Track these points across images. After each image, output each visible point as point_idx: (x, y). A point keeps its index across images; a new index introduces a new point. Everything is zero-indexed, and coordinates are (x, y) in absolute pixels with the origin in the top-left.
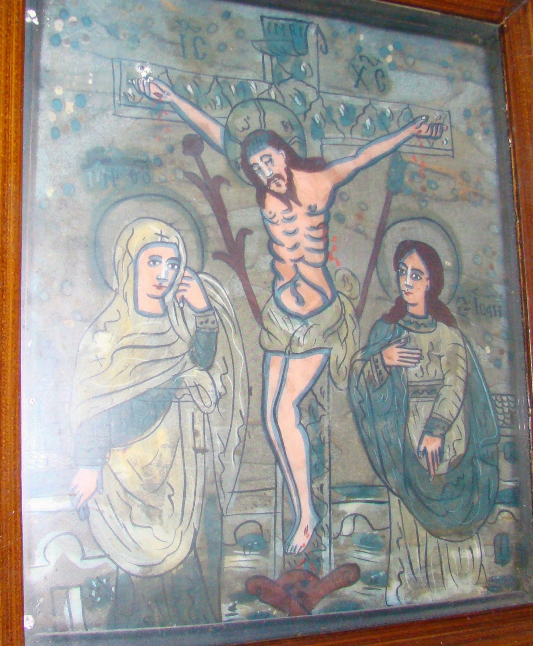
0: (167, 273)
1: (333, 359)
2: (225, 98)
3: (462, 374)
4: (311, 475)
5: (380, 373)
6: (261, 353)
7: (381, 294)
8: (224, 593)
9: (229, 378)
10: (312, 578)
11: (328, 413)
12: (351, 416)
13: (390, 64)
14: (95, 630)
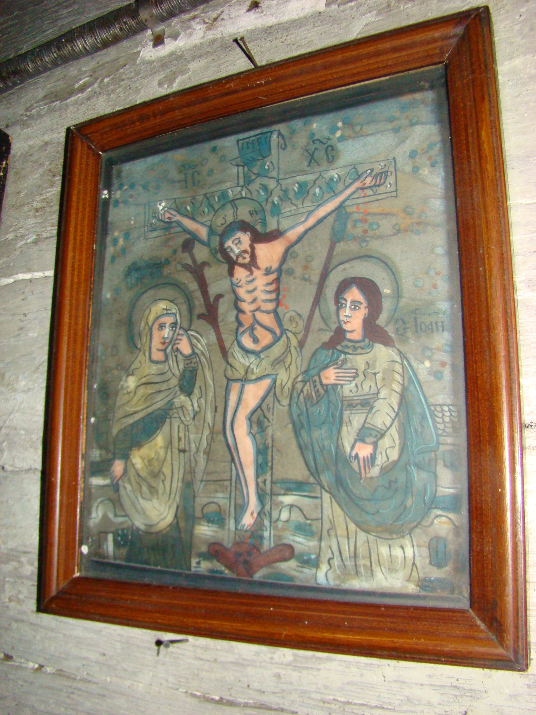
0: (169, 333)
1: (278, 382)
2: (211, 206)
3: (397, 388)
4: (257, 471)
5: (318, 391)
6: (225, 382)
7: (323, 326)
8: (194, 551)
9: (203, 401)
10: (255, 551)
11: (272, 425)
12: (290, 426)
13: (338, 138)
14: (118, 562)
